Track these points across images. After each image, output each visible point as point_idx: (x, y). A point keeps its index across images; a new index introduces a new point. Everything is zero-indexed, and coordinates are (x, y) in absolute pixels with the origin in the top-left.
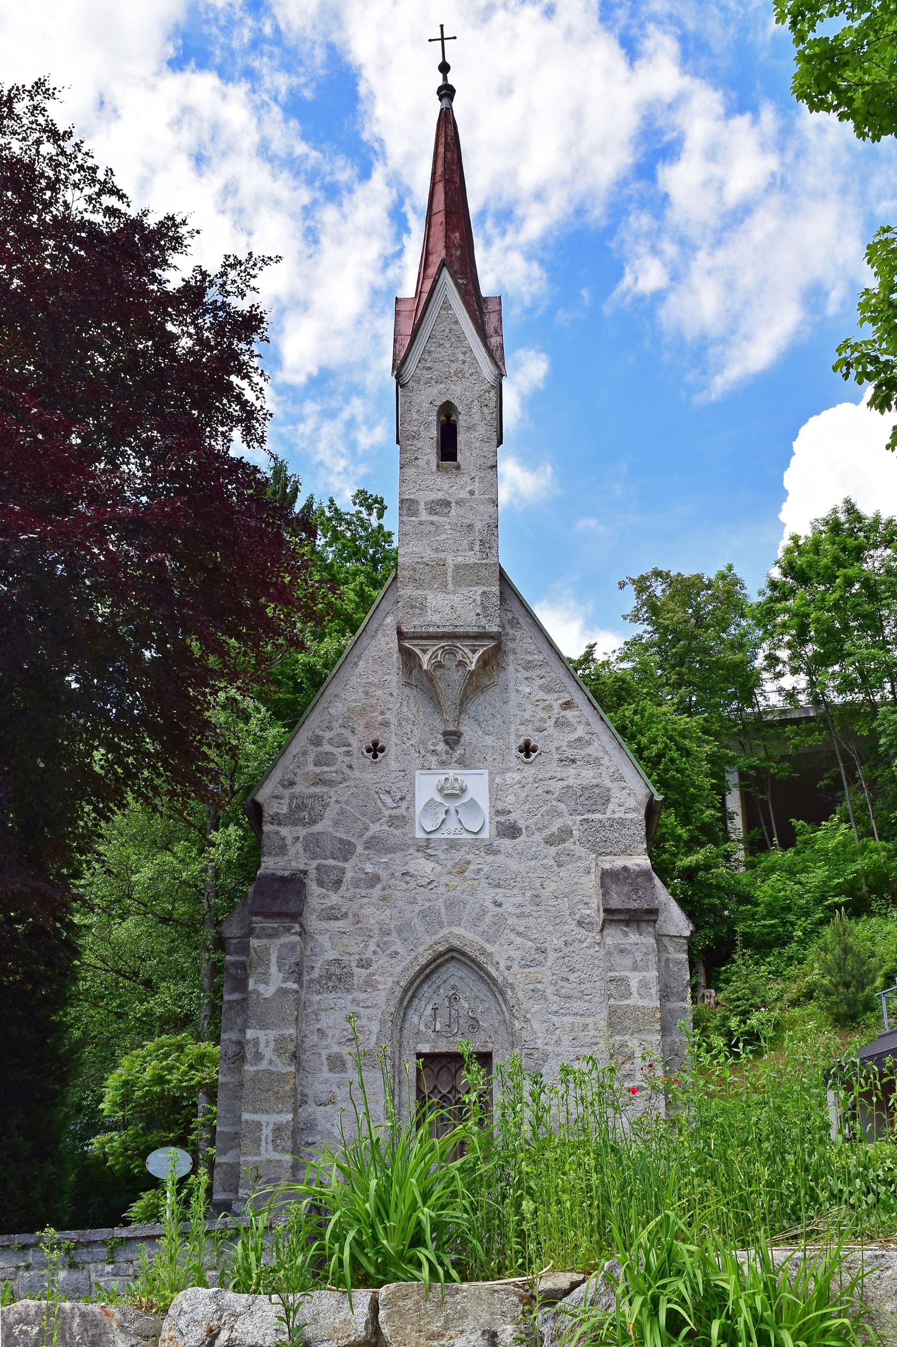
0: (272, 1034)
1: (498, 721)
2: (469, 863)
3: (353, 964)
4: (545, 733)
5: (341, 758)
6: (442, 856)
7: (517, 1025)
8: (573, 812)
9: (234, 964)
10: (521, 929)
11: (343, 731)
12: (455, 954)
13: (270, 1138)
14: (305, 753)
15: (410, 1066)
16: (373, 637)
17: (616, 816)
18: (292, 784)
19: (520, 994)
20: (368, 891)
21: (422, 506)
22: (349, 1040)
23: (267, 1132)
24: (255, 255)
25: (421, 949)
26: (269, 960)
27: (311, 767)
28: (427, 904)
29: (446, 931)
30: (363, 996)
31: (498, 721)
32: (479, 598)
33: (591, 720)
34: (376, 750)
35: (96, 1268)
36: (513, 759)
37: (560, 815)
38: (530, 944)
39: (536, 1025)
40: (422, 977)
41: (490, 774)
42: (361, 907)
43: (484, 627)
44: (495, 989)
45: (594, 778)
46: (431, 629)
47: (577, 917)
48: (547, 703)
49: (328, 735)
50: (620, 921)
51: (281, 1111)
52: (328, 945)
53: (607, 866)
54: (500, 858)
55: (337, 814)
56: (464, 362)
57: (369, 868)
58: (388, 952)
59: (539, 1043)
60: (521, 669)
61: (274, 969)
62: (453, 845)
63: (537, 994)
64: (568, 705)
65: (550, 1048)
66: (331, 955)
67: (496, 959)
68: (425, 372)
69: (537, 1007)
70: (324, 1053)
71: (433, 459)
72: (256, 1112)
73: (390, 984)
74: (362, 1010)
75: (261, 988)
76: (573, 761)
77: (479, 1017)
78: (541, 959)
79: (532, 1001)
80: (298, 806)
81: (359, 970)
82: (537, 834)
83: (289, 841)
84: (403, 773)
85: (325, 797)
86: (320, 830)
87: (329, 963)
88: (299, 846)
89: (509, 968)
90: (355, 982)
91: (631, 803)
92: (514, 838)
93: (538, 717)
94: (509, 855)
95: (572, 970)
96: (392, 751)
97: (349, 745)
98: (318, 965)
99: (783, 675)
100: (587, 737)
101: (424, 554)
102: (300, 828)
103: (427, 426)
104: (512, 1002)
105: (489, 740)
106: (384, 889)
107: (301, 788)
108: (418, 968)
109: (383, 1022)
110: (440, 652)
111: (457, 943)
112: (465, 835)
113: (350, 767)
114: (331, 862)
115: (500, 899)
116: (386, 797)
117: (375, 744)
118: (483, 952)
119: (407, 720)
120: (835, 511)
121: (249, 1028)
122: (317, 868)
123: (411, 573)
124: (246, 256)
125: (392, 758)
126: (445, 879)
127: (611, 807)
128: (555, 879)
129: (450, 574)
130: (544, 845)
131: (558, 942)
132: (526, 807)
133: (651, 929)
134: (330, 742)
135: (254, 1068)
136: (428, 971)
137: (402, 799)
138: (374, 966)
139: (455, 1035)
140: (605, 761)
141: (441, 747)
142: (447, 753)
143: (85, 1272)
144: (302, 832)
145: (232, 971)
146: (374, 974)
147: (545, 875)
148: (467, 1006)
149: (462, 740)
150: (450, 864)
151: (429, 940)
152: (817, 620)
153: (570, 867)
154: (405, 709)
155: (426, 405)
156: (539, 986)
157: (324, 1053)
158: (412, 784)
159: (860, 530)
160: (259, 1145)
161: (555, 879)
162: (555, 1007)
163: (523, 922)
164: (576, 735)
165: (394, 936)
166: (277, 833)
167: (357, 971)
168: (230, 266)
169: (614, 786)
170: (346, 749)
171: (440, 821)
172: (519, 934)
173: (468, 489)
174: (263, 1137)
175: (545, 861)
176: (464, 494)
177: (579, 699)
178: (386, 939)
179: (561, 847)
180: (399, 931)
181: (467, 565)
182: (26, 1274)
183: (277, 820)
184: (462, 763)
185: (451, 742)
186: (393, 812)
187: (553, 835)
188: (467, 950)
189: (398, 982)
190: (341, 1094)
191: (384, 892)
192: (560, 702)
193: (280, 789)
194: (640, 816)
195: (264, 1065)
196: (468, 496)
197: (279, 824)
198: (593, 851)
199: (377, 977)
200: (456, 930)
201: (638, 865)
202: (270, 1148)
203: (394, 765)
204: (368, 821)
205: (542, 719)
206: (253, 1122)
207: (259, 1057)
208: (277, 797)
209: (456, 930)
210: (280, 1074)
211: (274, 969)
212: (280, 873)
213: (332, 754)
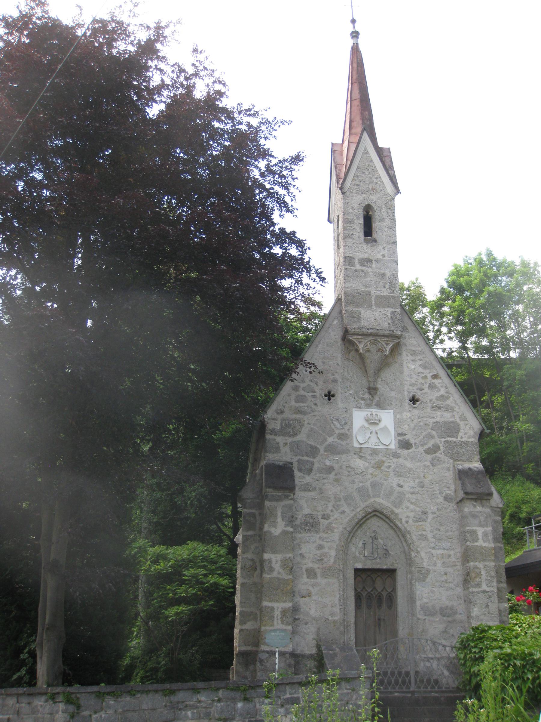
0: (279, 557)
1: (398, 383)
2: (383, 462)
3: (320, 517)
4: (424, 391)
5: (310, 399)
6: (369, 458)
7: (413, 554)
8: (441, 436)
9: (249, 514)
10: (413, 501)
11: (310, 383)
12: (377, 513)
13: (279, 617)
14: (289, 395)
15: (351, 575)
16: (326, 331)
17: (463, 440)
18: (282, 412)
19: (414, 537)
20: (327, 475)
21: (356, 261)
22: (318, 560)
23: (277, 613)
24: (278, 119)
25: (358, 510)
26: (276, 514)
27: (293, 403)
28: (361, 485)
29: (372, 500)
30: (325, 535)
31: (398, 383)
32: (389, 315)
33: (448, 385)
34: (330, 396)
35: (259, 700)
36: (407, 405)
37: (433, 437)
38: (418, 509)
39: (423, 554)
40: (358, 526)
41: (394, 412)
42: (324, 484)
43: (393, 331)
44: (399, 533)
45: (451, 418)
46: (364, 330)
47: (444, 495)
48: (424, 375)
49: (302, 385)
50: (472, 499)
51: (285, 601)
52: (305, 506)
53: (460, 467)
54: (401, 460)
55: (309, 431)
56: (377, 183)
57: (328, 463)
58: (340, 511)
59: (425, 565)
60: (409, 355)
61: (279, 519)
62: (375, 452)
63: (424, 537)
64: (435, 376)
65: (431, 568)
66: (306, 511)
67: (400, 517)
68: (355, 187)
69: (423, 545)
70: (304, 567)
71: (362, 234)
72: (271, 601)
73: (341, 529)
74: (325, 544)
75: (272, 530)
76: (439, 408)
77: (389, 549)
78: (425, 517)
79: (420, 541)
80: (286, 425)
82: (421, 448)
83: (281, 445)
84: (345, 410)
85: (302, 421)
86: (299, 439)
87: (306, 516)
88: (287, 448)
89: (407, 522)
90: (321, 527)
91: (471, 433)
92: (408, 449)
93: (419, 382)
94: (406, 459)
95: (442, 525)
96: (339, 397)
97: (315, 392)
98: (299, 517)
99: (445, 341)
100: (447, 395)
101: (358, 288)
102: (287, 438)
103: (358, 216)
104: (410, 541)
105: (393, 394)
106: (336, 475)
107: (288, 415)
108: (357, 520)
109: (337, 551)
110: (368, 343)
111: (378, 507)
112: (381, 447)
113: (316, 404)
114: (306, 458)
115: (401, 483)
116: (336, 423)
117: (329, 392)
118: (393, 512)
119: (347, 379)
120: (480, 254)
121: (266, 553)
122: (298, 461)
123: (352, 298)
124: (273, 119)
125: (339, 402)
126: (370, 471)
127: (461, 434)
128: (431, 473)
129: (373, 300)
130: (424, 454)
131: (434, 509)
132: (414, 432)
133: (488, 504)
134: (304, 389)
135: (269, 576)
136: (361, 522)
137: (346, 424)
140: (456, 409)
141: (367, 396)
142: (370, 400)
143: (253, 703)
144: (289, 440)
145: (248, 518)
146: (332, 523)
147: (425, 471)
148: (382, 542)
149: (378, 393)
150: (373, 462)
151: (362, 505)
152: (470, 314)
153: (439, 467)
154: (346, 373)
155: (356, 205)
156: (424, 533)
157: (304, 567)
158: (351, 415)
159: (494, 266)
160: (273, 620)
161: (431, 473)
162: (433, 545)
163: (414, 496)
164: (439, 394)
165: (343, 502)
166: (274, 440)
167: (322, 521)
168: (263, 123)
169: (462, 423)
170: (313, 394)
171: (367, 438)
172: (412, 503)
173: (382, 253)
174: (275, 616)
175: (426, 463)
176: (379, 256)
177: (442, 373)
178: (338, 503)
179: (434, 455)
180: (346, 499)
181: (382, 296)
182: (219, 705)
183: (274, 432)
184: (379, 406)
185: (372, 393)
186: (340, 431)
187: (429, 448)
188: (385, 511)
189: (345, 528)
190: (314, 591)
191: (337, 477)
192: (431, 374)
193: (276, 414)
194: (475, 440)
195: (275, 574)
196: (381, 257)
197: (275, 435)
198: (451, 458)
199: (333, 525)
200: (377, 500)
201: (476, 467)
202: (280, 622)
203: (340, 405)
204: (326, 436)
205: (422, 384)
206: (269, 607)
207: (271, 570)
208: (274, 419)
209: (377, 500)
210: (284, 579)
211: (279, 519)
212: (277, 463)
213: (305, 396)
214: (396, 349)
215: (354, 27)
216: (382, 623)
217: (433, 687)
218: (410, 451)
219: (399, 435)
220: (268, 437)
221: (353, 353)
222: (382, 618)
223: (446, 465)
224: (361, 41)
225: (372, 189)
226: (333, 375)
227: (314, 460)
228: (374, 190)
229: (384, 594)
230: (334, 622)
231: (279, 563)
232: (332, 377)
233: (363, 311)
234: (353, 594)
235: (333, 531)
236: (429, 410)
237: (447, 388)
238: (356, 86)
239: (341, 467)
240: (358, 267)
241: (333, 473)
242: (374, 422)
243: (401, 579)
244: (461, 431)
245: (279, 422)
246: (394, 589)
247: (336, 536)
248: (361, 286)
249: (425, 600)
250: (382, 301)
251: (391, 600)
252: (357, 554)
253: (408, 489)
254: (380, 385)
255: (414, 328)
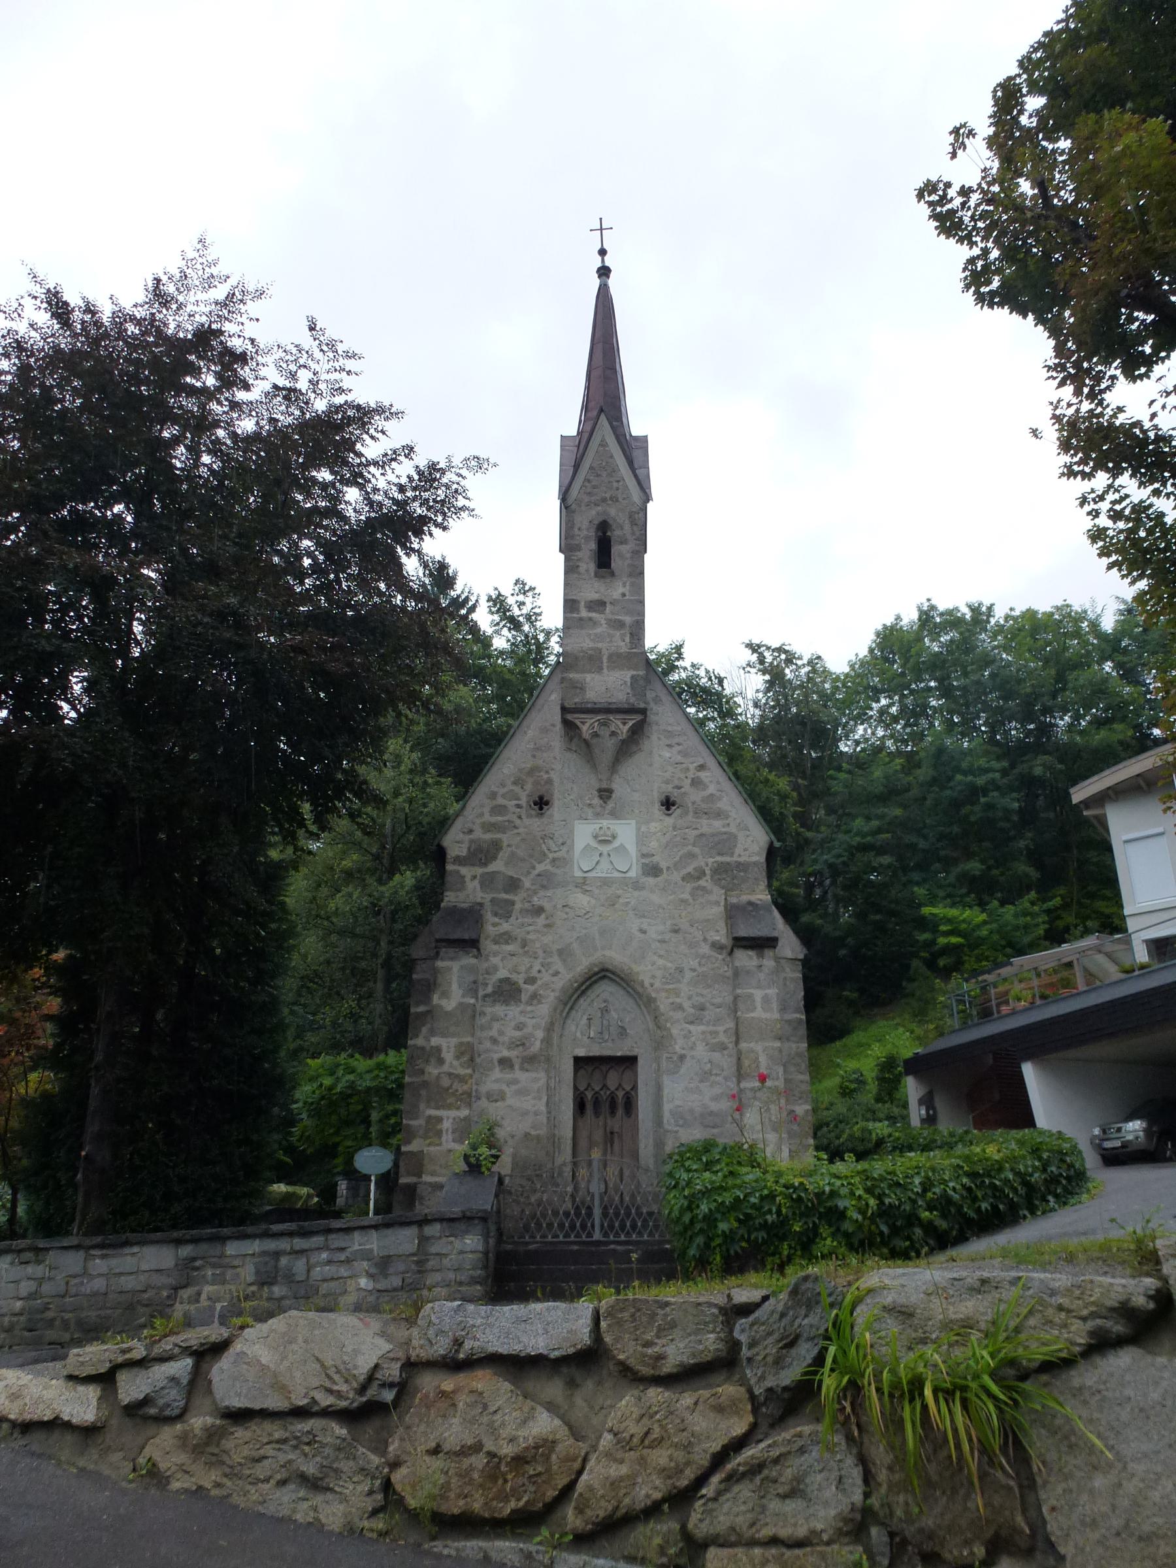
0: (454, 1041)
6: (597, 891)
10: (662, 953)
11: (514, 788)
15: (568, 1067)
17: (741, 860)
18: (471, 831)
30: (529, 1008)
33: (721, 780)
36: (657, 812)
38: (669, 965)
58: (551, 972)
62: (605, 882)
64: (702, 767)
71: (592, 566)
72: (437, 1108)
81: (526, 986)
86: (495, 869)
87: (501, 981)
91: (755, 848)
92: (656, 876)
94: (652, 891)
97: (518, 799)
100: (718, 794)
112: (617, 874)
113: (520, 817)
115: (645, 927)
117: (541, 798)
122: (493, 900)
125: (556, 811)
134: (504, 796)
138: (539, 982)
139: (606, 1041)
141: (596, 801)
144: (479, 871)
158: (572, 832)
172: (661, 956)
184: (614, 815)
186: (555, 855)
193: (461, 835)
194: (762, 858)
211: (455, 986)
213: (505, 806)
214: (638, 732)
215: (603, 261)
216: (616, 1140)
217: (567, 1235)
218: (659, 879)
219: (644, 856)
220: (450, 867)
221: (575, 740)
222: (616, 1130)
223: (713, 898)
224: (612, 282)
225: (611, 498)
226: (547, 772)
227: (516, 898)
228: (614, 499)
229: (620, 1094)
230: (538, 1137)
231: (453, 1049)
232: (546, 776)
233: (588, 677)
234: (571, 1094)
235: (540, 1002)
236: (690, 817)
237: (718, 783)
238: (600, 346)
239: (555, 906)
240: (584, 613)
241: (543, 916)
242: (605, 840)
243: (644, 1069)
244: (739, 845)
245: (465, 846)
246: (635, 1087)
247: (544, 1010)
248: (588, 641)
249: (678, 1103)
250: (618, 661)
251: (630, 1105)
252: (578, 1034)
253: (654, 936)
254: (618, 785)
255: (670, 699)
